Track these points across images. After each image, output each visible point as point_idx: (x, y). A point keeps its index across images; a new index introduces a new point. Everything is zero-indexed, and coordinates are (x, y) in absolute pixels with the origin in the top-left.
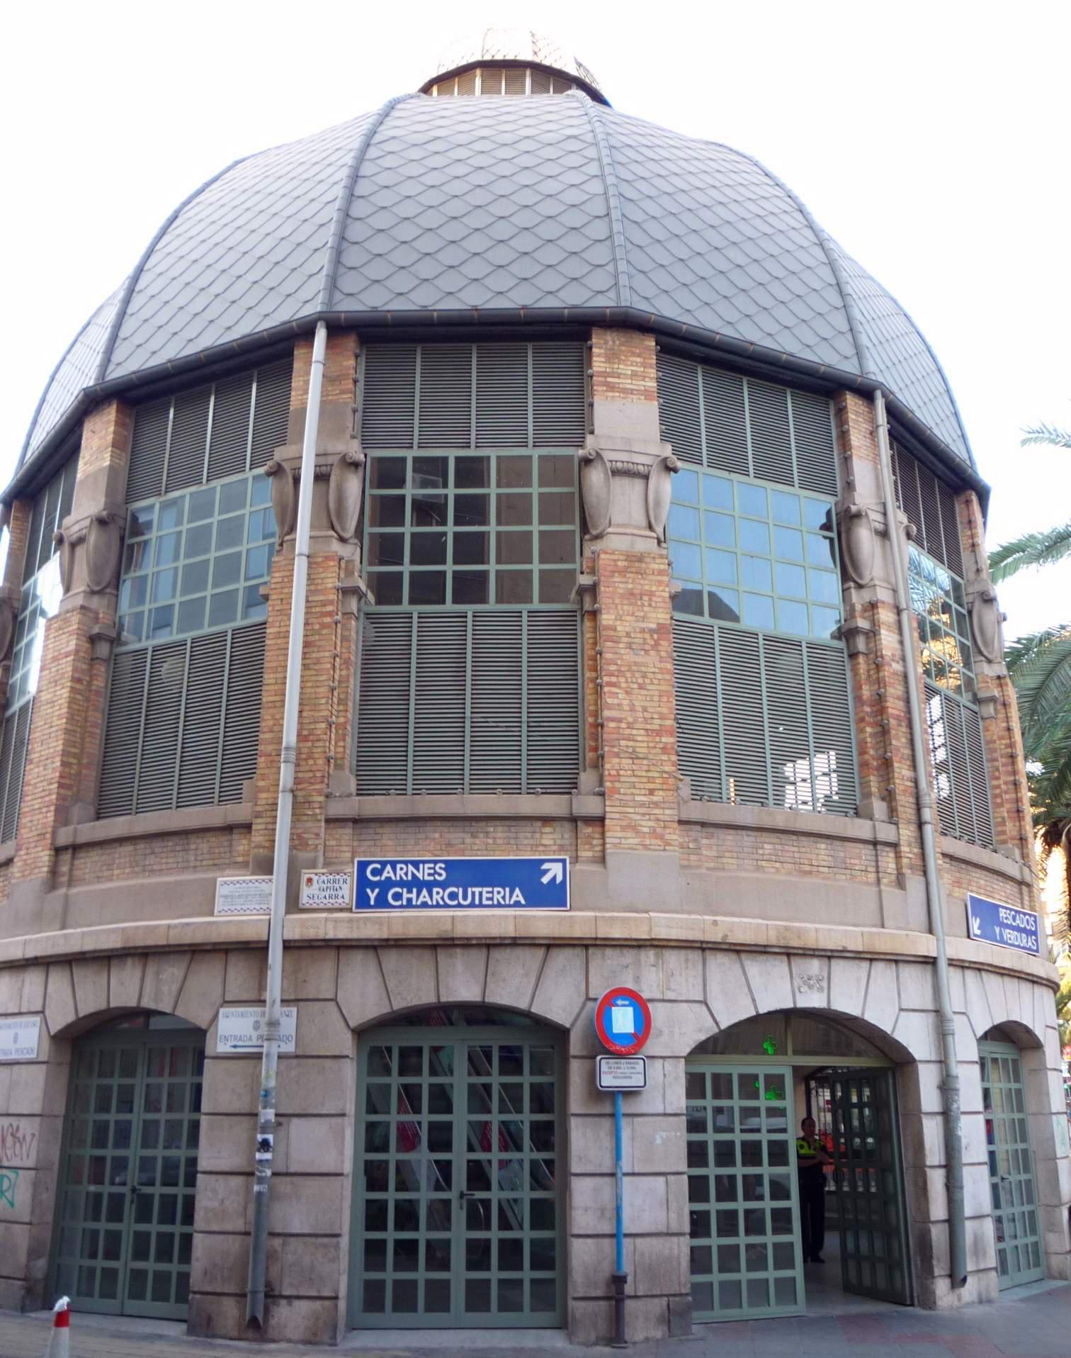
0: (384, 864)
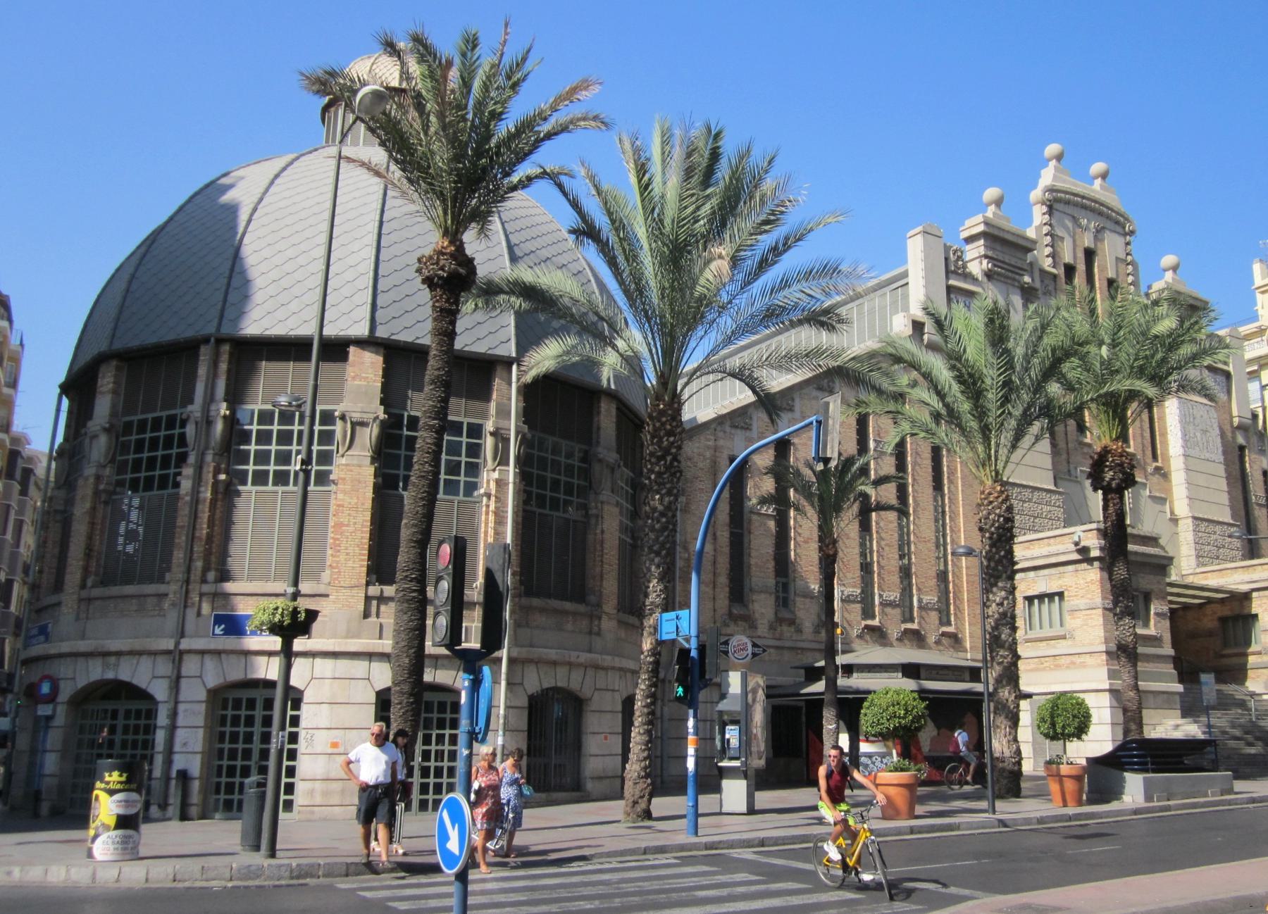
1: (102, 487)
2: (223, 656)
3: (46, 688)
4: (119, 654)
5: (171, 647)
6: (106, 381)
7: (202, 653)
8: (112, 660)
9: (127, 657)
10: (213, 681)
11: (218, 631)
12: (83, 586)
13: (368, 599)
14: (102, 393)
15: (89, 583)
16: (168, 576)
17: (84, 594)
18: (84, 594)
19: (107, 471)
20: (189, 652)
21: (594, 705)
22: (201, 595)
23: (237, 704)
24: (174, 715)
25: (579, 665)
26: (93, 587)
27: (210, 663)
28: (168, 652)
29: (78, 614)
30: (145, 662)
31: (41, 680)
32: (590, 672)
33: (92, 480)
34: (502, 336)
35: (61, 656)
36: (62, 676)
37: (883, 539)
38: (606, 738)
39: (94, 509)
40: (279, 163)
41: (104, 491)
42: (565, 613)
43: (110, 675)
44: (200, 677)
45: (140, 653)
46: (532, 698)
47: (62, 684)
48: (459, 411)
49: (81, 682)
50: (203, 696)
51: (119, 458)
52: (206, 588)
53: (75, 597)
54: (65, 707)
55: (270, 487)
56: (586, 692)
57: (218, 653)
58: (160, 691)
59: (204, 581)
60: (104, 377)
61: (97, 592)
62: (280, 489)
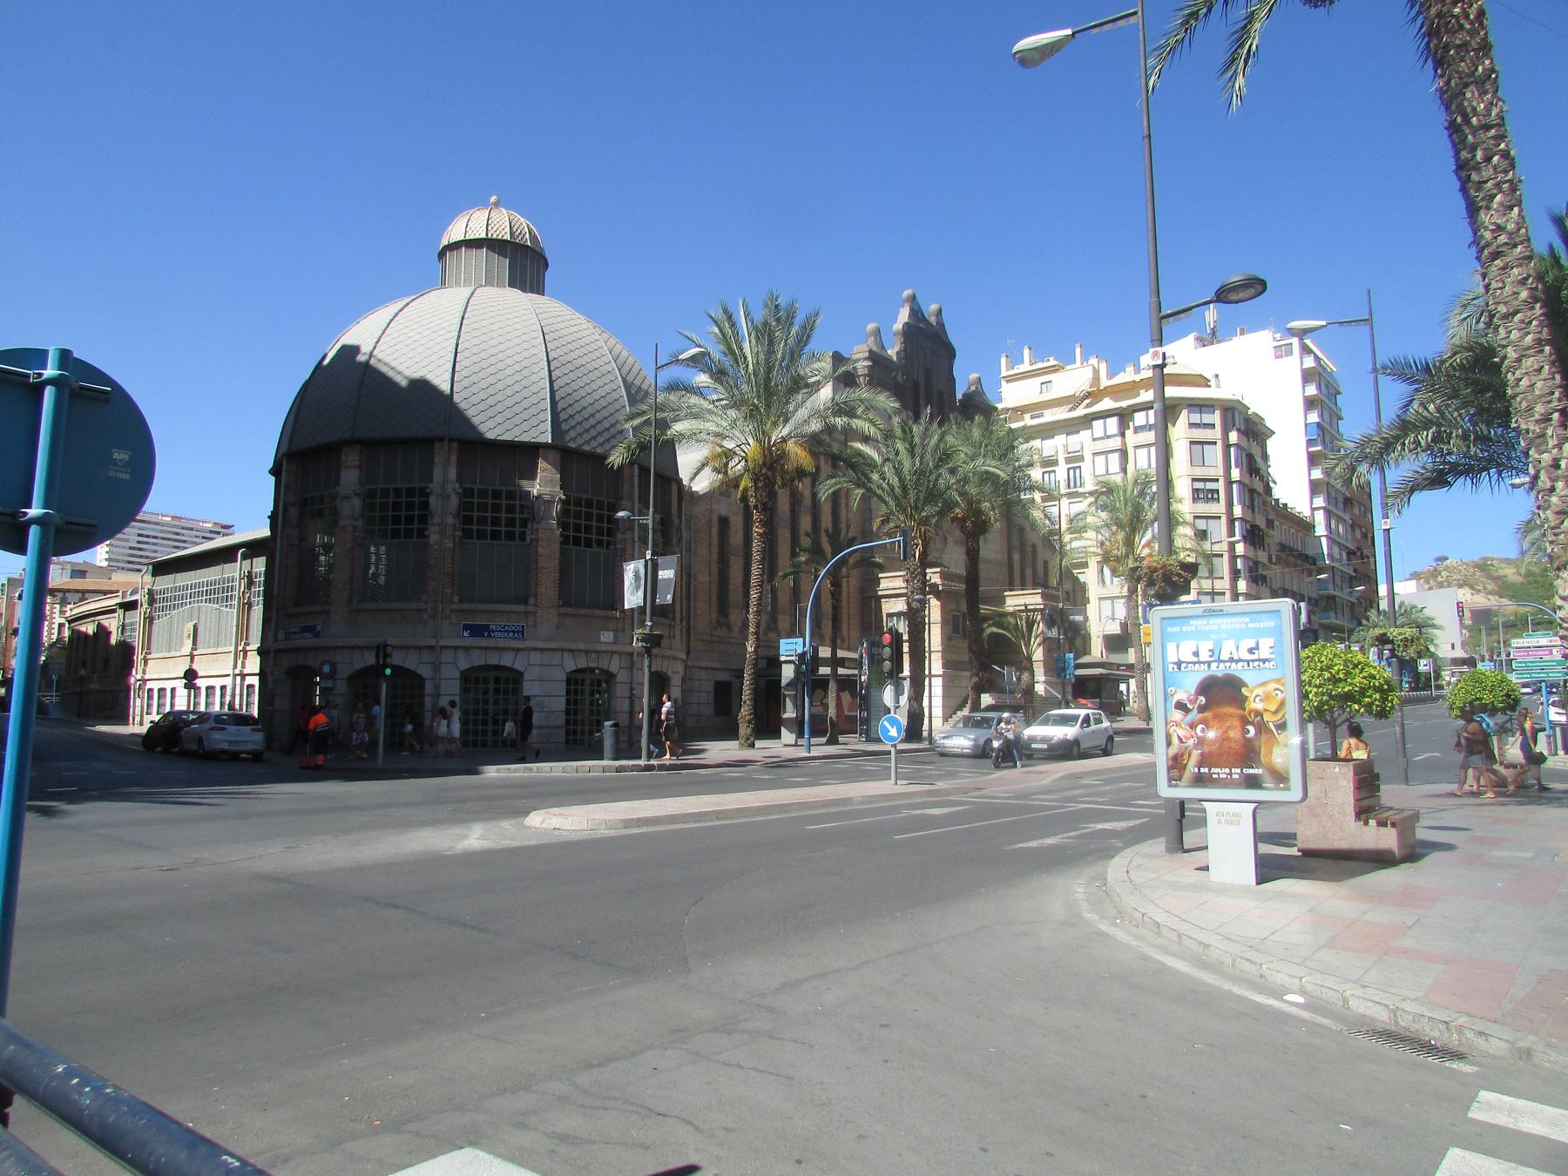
7: (456, 648)
10: (464, 664)
12: (350, 601)
19: (359, 523)
21: (526, 677)
23: (477, 681)
24: (437, 687)
27: (460, 654)
31: (323, 663)
34: (542, 427)
35: (337, 648)
38: (1196, 654)
40: (400, 305)
42: (593, 616)
45: (408, 648)
46: (462, 672)
47: (339, 667)
48: (875, 650)
50: (457, 675)
56: (518, 666)
57: (466, 648)
58: (425, 671)
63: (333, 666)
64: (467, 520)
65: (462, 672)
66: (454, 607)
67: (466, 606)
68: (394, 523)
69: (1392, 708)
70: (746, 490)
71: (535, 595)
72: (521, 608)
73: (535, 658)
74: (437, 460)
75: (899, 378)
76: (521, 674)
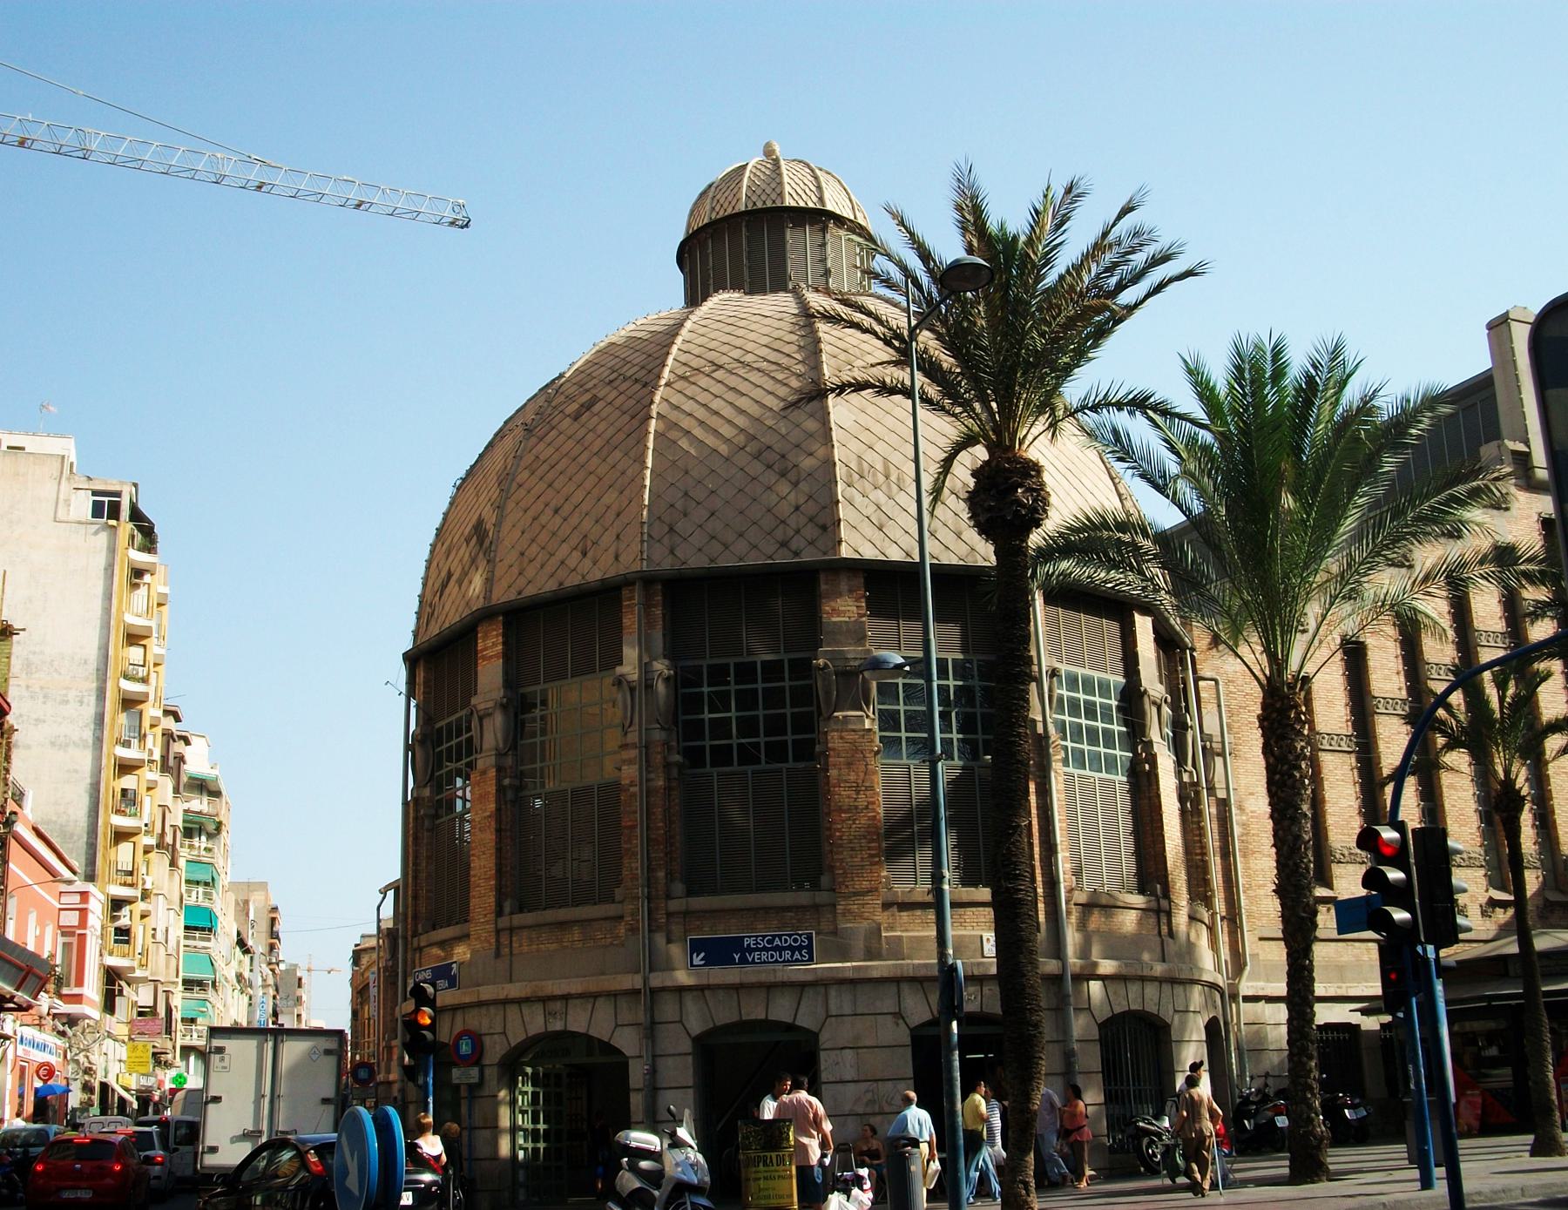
0: (774, 937)
1: (507, 782)
2: (707, 993)
3: (465, 1048)
4: (566, 998)
5: (639, 984)
6: (489, 643)
8: (558, 1005)
9: (577, 1002)
10: (696, 1026)
11: (697, 961)
12: (499, 913)
13: (498, 932)
14: (485, 658)
15: (507, 909)
16: (618, 893)
17: (504, 922)
18: (504, 922)
20: (663, 989)
21: (825, 1039)
22: (669, 915)
25: (1153, 979)
26: (512, 913)
28: (636, 992)
29: (498, 949)
30: (604, 1011)
32: (1166, 988)
33: (492, 773)
36: (484, 1031)
37: (66, 932)
39: (498, 810)
41: (511, 786)
43: (557, 1026)
44: (681, 1021)
46: (698, 1041)
47: (487, 1040)
49: (516, 1037)
50: (687, 1046)
51: (682, 718)
52: (674, 905)
53: (491, 927)
54: (495, 1069)
55: (735, 768)
56: (804, 1021)
58: (627, 1042)
59: (668, 897)
60: (485, 638)
61: (518, 919)
62: (749, 769)
63: (477, 1039)
64: (694, 730)
65: (698, 1041)
66: (674, 905)
67: (699, 902)
68: (910, 717)
69: (468, 541)
70: (1203, 1177)
71: (832, 868)
72: (804, 898)
73: (839, 1001)
74: (626, 621)
75: (815, 1154)
76: (815, 1036)
